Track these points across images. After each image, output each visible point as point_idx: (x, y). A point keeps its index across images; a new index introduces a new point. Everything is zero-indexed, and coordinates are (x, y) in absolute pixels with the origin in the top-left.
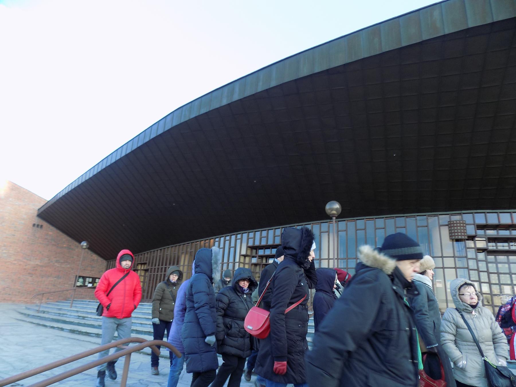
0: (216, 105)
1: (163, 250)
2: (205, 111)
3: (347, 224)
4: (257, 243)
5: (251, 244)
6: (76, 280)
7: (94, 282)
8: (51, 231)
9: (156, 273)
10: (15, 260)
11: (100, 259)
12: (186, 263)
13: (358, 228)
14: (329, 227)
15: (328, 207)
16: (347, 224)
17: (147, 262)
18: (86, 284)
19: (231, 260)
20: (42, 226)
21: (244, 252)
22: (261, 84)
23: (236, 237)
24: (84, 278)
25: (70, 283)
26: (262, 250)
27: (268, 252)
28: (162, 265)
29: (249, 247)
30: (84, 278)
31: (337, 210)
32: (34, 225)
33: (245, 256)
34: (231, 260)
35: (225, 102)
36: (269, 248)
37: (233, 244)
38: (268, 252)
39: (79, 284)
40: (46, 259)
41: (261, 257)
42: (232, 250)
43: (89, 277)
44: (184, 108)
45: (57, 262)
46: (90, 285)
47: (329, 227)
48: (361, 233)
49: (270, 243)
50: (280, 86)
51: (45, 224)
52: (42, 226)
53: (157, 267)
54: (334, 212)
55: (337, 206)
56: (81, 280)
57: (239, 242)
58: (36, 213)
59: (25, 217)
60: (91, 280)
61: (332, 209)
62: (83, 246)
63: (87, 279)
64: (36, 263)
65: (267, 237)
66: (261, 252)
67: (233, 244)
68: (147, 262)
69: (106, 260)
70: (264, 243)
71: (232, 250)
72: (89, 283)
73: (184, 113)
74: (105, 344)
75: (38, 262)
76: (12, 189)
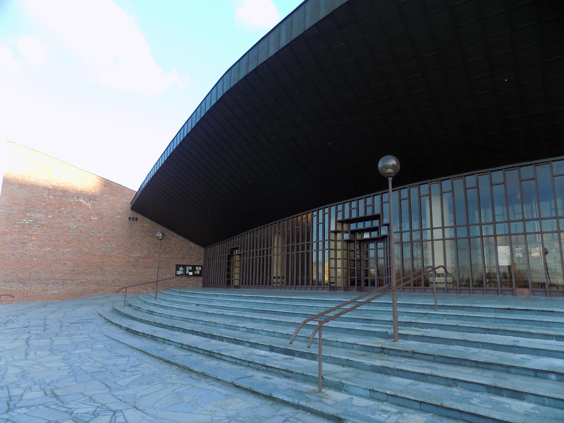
0: (263, 59)
1: (259, 230)
2: (253, 68)
3: (452, 183)
4: (347, 217)
5: (340, 218)
6: (178, 269)
7: (194, 270)
8: (146, 223)
9: (251, 257)
10: (119, 254)
11: (197, 247)
12: (280, 245)
13: (467, 186)
14: (430, 188)
15: (380, 165)
16: (452, 183)
17: (239, 246)
18: (187, 272)
19: (321, 238)
20: (137, 219)
21: (333, 228)
22: (308, 18)
23: (337, 208)
24: (184, 267)
25: (171, 272)
26: (354, 224)
27: (360, 226)
28: (298, 241)
29: (339, 222)
30: (184, 267)
31: (393, 167)
32: (130, 218)
33: (336, 232)
34: (321, 238)
35: (272, 52)
36: (354, 222)
37: (321, 221)
38: (360, 226)
39: (179, 273)
40: (146, 250)
41: (353, 232)
42: (321, 226)
43: (189, 266)
44: (233, 69)
45: (156, 252)
46: (191, 274)
47: (430, 188)
48: (499, 190)
49: (362, 214)
50: (331, 16)
51: (139, 216)
52: (137, 219)
53: (248, 251)
54: (390, 171)
55: (393, 162)
56: (181, 268)
57: (327, 216)
58: (129, 207)
59: (120, 211)
60: (191, 268)
61: (387, 167)
62: (158, 237)
63: (187, 268)
64: (138, 255)
65: (373, 205)
66: (353, 227)
67: (321, 221)
68: (239, 246)
69: (203, 247)
70: (354, 216)
71: (321, 226)
72: (190, 271)
73: (233, 76)
74: (515, 273)
75: (139, 254)
76: (105, 186)
